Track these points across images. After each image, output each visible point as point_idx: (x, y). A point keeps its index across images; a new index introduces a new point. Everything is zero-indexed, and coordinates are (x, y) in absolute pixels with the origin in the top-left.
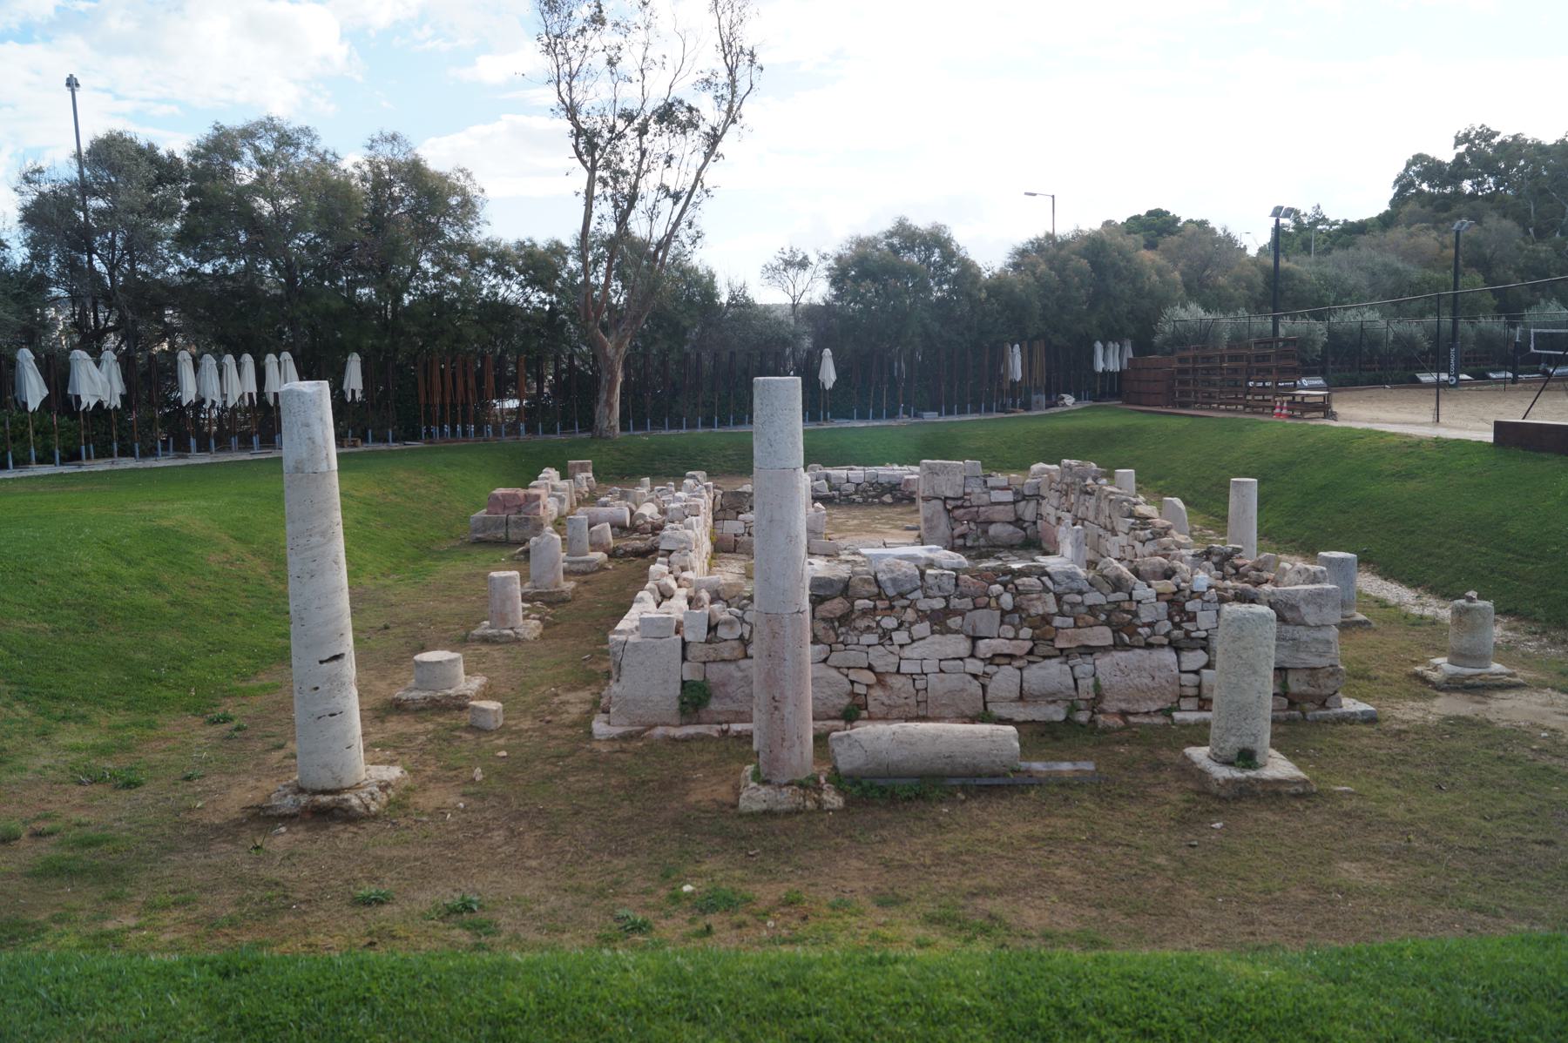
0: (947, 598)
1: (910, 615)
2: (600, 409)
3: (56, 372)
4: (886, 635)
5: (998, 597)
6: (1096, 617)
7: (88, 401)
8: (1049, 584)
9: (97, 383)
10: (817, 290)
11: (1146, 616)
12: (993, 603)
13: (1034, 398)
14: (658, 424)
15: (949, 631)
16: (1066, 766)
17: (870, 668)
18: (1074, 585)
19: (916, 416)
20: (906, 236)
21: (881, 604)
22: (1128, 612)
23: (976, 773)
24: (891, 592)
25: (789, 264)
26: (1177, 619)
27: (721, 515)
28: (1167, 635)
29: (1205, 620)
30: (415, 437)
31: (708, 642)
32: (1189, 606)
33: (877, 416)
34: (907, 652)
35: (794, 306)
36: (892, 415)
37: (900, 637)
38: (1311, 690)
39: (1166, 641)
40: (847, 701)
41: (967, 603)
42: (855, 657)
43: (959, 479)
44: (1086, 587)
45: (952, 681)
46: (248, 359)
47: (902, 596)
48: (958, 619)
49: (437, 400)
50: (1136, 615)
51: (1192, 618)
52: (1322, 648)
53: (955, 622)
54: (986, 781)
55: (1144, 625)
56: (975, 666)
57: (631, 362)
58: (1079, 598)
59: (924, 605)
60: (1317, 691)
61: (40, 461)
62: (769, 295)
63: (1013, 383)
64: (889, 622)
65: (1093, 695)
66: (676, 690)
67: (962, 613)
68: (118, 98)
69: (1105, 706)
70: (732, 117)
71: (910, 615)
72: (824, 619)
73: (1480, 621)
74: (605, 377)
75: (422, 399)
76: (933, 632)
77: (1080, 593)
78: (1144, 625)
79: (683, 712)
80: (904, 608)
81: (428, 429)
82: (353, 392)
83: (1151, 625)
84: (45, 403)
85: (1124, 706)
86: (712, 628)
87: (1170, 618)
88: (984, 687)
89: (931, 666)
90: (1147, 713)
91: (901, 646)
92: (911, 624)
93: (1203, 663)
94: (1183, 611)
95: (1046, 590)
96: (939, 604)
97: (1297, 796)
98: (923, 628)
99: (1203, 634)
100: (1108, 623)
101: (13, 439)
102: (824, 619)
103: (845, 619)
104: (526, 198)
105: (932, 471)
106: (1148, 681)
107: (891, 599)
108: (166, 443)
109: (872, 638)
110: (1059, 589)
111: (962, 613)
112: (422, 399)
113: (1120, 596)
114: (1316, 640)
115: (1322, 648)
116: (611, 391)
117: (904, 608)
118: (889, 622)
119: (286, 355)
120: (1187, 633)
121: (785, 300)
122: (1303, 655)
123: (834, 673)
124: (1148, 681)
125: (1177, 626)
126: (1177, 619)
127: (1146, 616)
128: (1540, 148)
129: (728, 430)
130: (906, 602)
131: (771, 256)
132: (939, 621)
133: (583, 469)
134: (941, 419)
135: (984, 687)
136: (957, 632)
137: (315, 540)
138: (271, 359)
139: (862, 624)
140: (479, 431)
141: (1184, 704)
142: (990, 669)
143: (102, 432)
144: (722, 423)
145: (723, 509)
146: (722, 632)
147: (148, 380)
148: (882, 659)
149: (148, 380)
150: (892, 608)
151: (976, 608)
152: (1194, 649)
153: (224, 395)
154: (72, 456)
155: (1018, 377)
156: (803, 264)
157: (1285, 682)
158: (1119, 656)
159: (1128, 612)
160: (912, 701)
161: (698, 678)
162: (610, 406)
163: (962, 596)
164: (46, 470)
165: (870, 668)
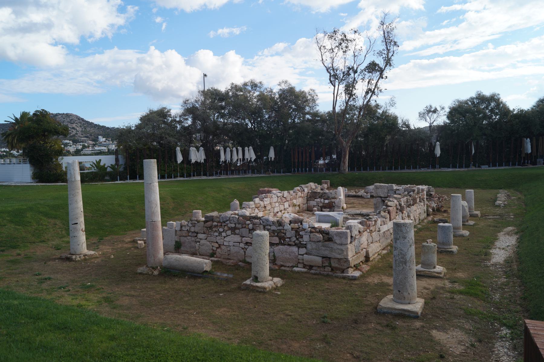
0: (235, 224)
1: (226, 228)
2: (342, 164)
3: (186, 154)
4: (220, 233)
5: (248, 225)
6: (274, 234)
7: (193, 161)
8: (262, 222)
9: (197, 156)
10: (441, 119)
11: (288, 235)
12: (247, 227)
13: (538, 160)
14: (372, 169)
15: (235, 234)
16: (226, 275)
17: (217, 242)
18: (268, 223)
19: (479, 167)
20: (481, 99)
21: (219, 224)
22: (283, 233)
23: (194, 272)
24: (221, 221)
25: (429, 111)
26: (298, 237)
27: (309, 199)
28: (294, 242)
29: (306, 238)
30: (290, 172)
31: (180, 230)
32: (301, 233)
33: (461, 167)
34: (225, 239)
35: (430, 126)
36: (467, 166)
37: (224, 234)
38: (339, 266)
39: (294, 244)
40: (211, 251)
41: (240, 226)
42: (213, 239)
43: (386, 191)
44: (271, 224)
45: (236, 249)
46: (240, 149)
47: (224, 222)
48: (238, 231)
49: (296, 160)
50: (285, 234)
51: (302, 237)
52: (340, 252)
53: (237, 231)
54: (196, 275)
55: (287, 238)
56: (242, 245)
57: (366, 149)
58: (269, 227)
59: (229, 225)
60: (341, 267)
61: (181, 176)
62: (417, 123)
63: (527, 154)
64: (221, 230)
65: (273, 258)
66: (174, 243)
67: (239, 229)
68: (295, 69)
69: (276, 262)
70: (330, 79)
71: (226, 228)
72: (206, 227)
73: (427, 251)
74: (343, 153)
75: (292, 160)
76: (232, 234)
77: (270, 226)
78: (287, 238)
79: (175, 250)
80: (225, 226)
81: (294, 170)
82: (271, 158)
83: (290, 238)
84: (182, 162)
85: (282, 263)
86: (181, 227)
87: (296, 237)
88: (245, 252)
89: (231, 244)
90: (289, 267)
91: (225, 237)
92: (227, 231)
93: (304, 252)
94: (299, 235)
95: (261, 224)
96: (233, 225)
97: (261, 292)
98: (229, 232)
99: (305, 243)
100: (277, 236)
101: (174, 171)
102: (206, 227)
103: (211, 228)
104: (326, 100)
105: (377, 188)
106: (288, 256)
107: (221, 223)
108: (194, 171)
109: (216, 234)
110: (264, 224)
111: (239, 229)
112: (292, 160)
113: (281, 228)
114: (338, 249)
115: (340, 252)
116: (345, 157)
117: (225, 226)
118: (221, 230)
119: (251, 147)
120: (300, 242)
121: (427, 125)
122: (334, 254)
123: (208, 243)
124: (288, 256)
125: (297, 239)
126: (298, 237)
127: (288, 235)
128: (108, 128)
129: (436, 170)
130: (225, 224)
131: (422, 109)
132: (233, 230)
133: (326, 183)
134: (490, 168)
135: (245, 252)
136: (237, 234)
137: (71, 196)
138: (246, 148)
139: (214, 229)
140: (310, 170)
141: (299, 265)
142: (246, 247)
143: (198, 169)
144: (395, 169)
145: (310, 197)
146: (183, 228)
147: (212, 155)
148: (220, 240)
149: (212, 155)
150: (221, 225)
151: (242, 228)
152: (303, 247)
153: (231, 160)
154: (189, 175)
155: (530, 151)
156: (435, 111)
157: (330, 263)
158: (281, 247)
159: (283, 233)
160: (227, 254)
161: (178, 240)
162: (344, 163)
163: (239, 224)
164: (182, 179)
165: (217, 242)
